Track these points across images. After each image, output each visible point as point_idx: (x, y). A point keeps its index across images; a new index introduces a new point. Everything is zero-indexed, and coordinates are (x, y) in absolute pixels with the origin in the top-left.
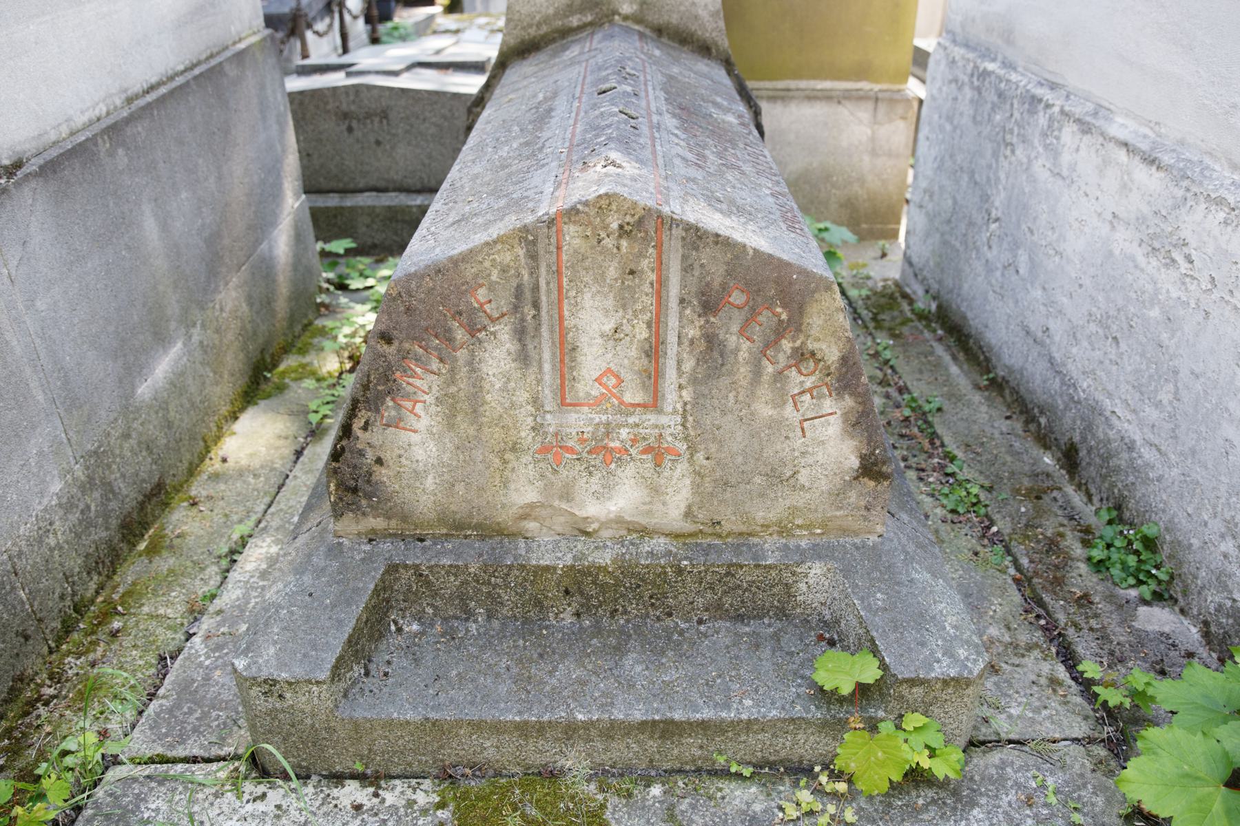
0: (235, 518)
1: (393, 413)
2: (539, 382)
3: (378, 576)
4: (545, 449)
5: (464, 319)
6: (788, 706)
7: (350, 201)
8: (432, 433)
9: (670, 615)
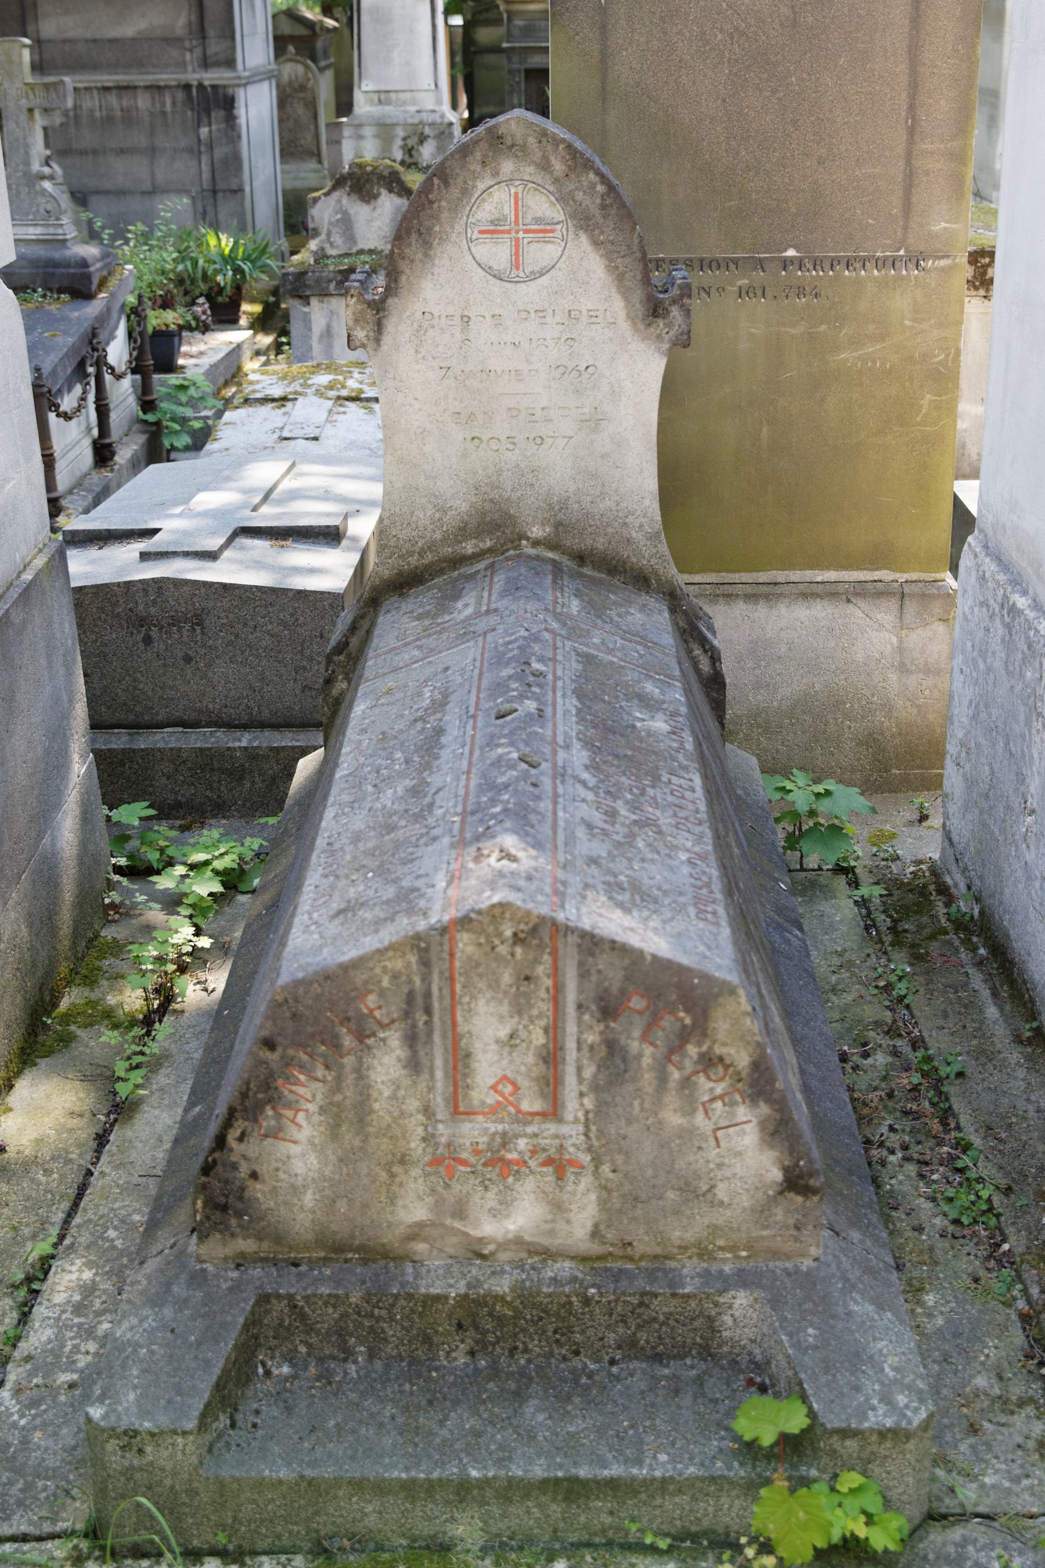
0: (26, 1231)
1: (273, 1123)
2: (430, 1089)
3: (248, 1308)
4: (436, 1162)
5: (353, 1025)
7: (145, 741)
8: (313, 1144)
9: (577, 1353)
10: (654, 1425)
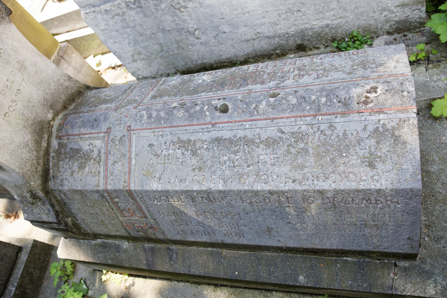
10: (434, 140)
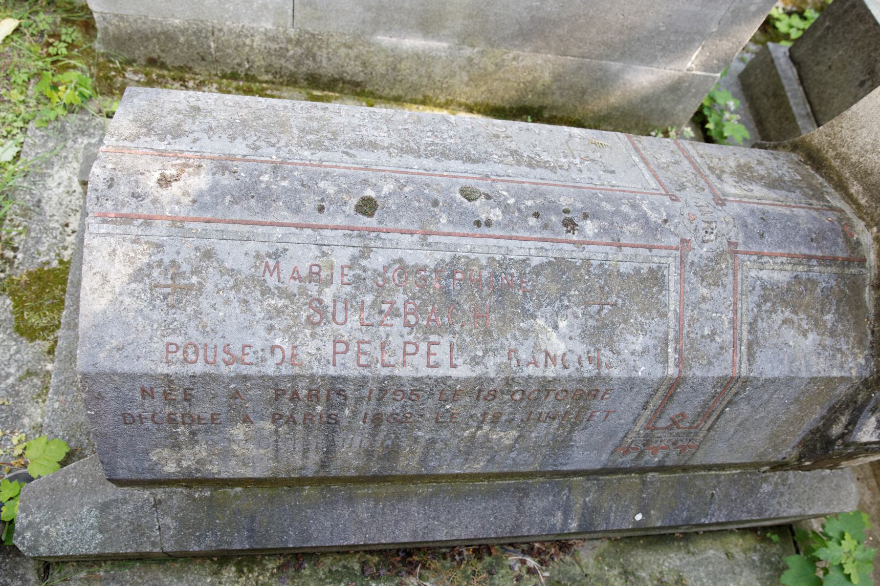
6: (50, 429)
